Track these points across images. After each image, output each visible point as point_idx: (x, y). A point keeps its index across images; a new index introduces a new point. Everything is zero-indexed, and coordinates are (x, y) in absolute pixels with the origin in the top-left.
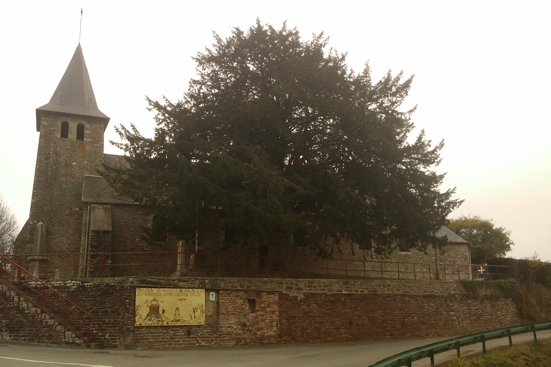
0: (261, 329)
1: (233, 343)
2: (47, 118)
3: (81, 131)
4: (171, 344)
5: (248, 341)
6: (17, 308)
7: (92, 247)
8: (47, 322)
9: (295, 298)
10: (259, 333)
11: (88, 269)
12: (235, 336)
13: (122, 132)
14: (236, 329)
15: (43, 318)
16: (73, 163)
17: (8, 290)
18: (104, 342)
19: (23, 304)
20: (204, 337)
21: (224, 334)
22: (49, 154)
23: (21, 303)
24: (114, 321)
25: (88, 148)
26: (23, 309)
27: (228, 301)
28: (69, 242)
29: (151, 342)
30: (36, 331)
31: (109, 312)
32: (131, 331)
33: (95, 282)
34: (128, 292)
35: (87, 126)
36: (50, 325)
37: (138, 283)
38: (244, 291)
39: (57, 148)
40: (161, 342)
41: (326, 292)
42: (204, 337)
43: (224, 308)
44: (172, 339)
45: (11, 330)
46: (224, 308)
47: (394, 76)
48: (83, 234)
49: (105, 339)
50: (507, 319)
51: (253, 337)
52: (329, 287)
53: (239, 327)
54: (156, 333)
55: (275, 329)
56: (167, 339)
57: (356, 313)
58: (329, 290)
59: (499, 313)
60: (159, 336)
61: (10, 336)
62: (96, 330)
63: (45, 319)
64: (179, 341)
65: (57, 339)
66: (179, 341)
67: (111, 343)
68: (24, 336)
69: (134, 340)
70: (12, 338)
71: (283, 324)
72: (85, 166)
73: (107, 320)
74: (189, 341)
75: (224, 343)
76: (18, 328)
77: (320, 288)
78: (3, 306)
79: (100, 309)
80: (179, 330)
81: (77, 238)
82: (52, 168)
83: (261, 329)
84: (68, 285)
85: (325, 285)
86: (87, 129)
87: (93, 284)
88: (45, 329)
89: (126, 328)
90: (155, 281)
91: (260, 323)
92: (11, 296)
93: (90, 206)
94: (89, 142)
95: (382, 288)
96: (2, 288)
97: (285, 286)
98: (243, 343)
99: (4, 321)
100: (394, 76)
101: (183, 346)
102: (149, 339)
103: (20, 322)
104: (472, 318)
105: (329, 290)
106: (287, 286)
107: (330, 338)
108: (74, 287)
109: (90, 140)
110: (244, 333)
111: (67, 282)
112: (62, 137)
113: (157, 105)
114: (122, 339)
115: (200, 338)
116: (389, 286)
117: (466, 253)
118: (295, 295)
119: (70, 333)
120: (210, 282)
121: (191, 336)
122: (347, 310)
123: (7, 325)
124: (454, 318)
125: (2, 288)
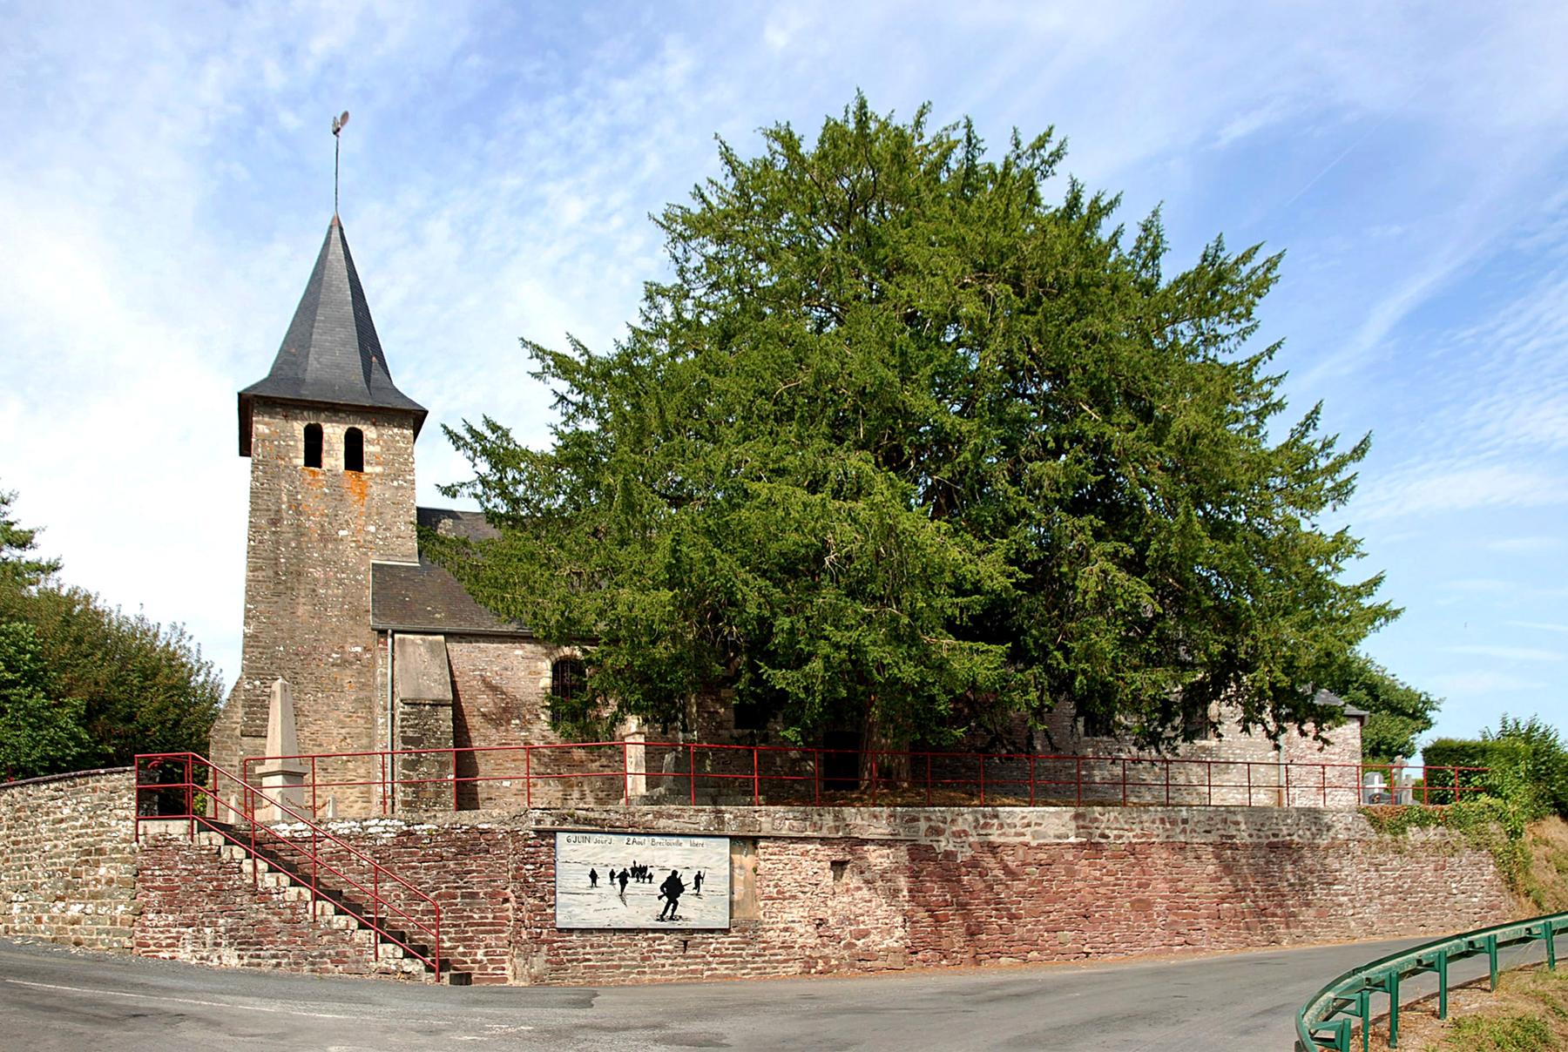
0: (866, 934)
1: (797, 967)
2: (267, 419)
3: (354, 443)
4: (644, 972)
5: (833, 962)
6: (253, 890)
7: (406, 740)
8: (329, 922)
9: (949, 855)
10: (860, 943)
11: (399, 796)
12: (799, 952)
13: (468, 440)
14: (805, 935)
15: (318, 912)
16: (341, 533)
17: (226, 844)
18: (473, 969)
19: (266, 879)
20: (725, 956)
21: (773, 948)
22: (279, 511)
23: (259, 876)
24: (494, 918)
25: (375, 490)
26: (268, 892)
27: (781, 866)
28: (343, 731)
29: (593, 967)
30: (304, 944)
31: (481, 895)
32: (544, 942)
33: (440, 821)
34: (530, 846)
35: (369, 432)
36: (337, 931)
37: (553, 823)
38: (822, 839)
39: (297, 493)
40: (619, 967)
41: (1027, 839)
42: (725, 956)
43: (772, 883)
44: (644, 959)
45: (239, 944)
46: (772, 883)
47: (1231, 254)
48: (378, 710)
49: (474, 962)
50: (1474, 900)
51: (846, 953)
52: (1037, 828)
53: (811, 929)
54: (604, 946)
55: (899, 933)
56: (633, 959)
57: (1102, 890)
58: (1035, 835)
59: (1454, 885)
60: (613, 953)
61: (240, 957)
62: (450, 939)
63: (323, 914)
64: (663, 966)
65: (358, 962)
66: (663, 966)
67: (489, 971)
68: (274, 956)
69: (552, 963)
70: (246, 961)
71: (917, 922)
72: (369, 538)
73: (476, 916)
74: (688, 965)
75: (776, 968)
76: (258, 937)
77: (1013, 830)
78: (215, 883)
79: (457, 888)
80: (662, 938)
81: (363, 721)
82: (287, 545)
83: (866, 934)
84: (371, 830)
85: (1026, 821)
86: (370, 442)
87: (435, 827)
88: (326, 938)
89: (530, 933)
90: (597, 815)
91: (861, 918)
92: (232, 858)
93: (393, 637)
94: (377, 475)
95: (1168, 826)
96: (210, 841)
97: (923, 825)
98: (819, 968)
99: (221, 921)
100: (1231, 254)
101: (675, 977)
102: (589, 960)
103: (261, 922)
104: (1389, 898)
105: (1035, 835)
106: (930, 827)
107: (1035, 954)
108: (387, 835)
109: (379, 469)
110: (824, 945)
111: (368, 823)
112: (307, 464)
113: (563, 366)
114: (519, 961)
115: (715, 956)
116: (1185, 821)
117: (1353, 741)
118: (950, 848)
119: (390, 947)
120: (735, 818)
121: (691, 952)
122: (1079, 885)
123: (232, 930)
124: (1344, 899)
125: (210, 841)
